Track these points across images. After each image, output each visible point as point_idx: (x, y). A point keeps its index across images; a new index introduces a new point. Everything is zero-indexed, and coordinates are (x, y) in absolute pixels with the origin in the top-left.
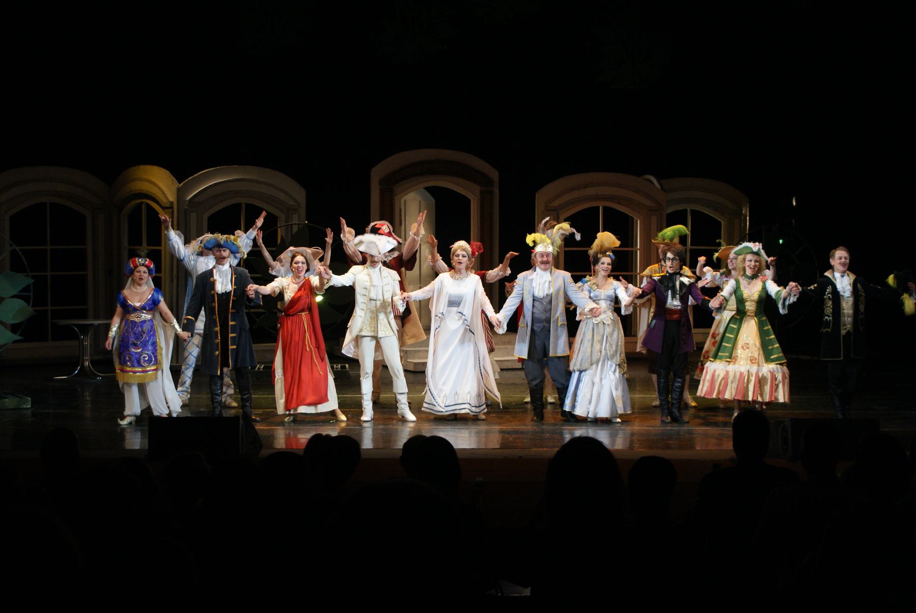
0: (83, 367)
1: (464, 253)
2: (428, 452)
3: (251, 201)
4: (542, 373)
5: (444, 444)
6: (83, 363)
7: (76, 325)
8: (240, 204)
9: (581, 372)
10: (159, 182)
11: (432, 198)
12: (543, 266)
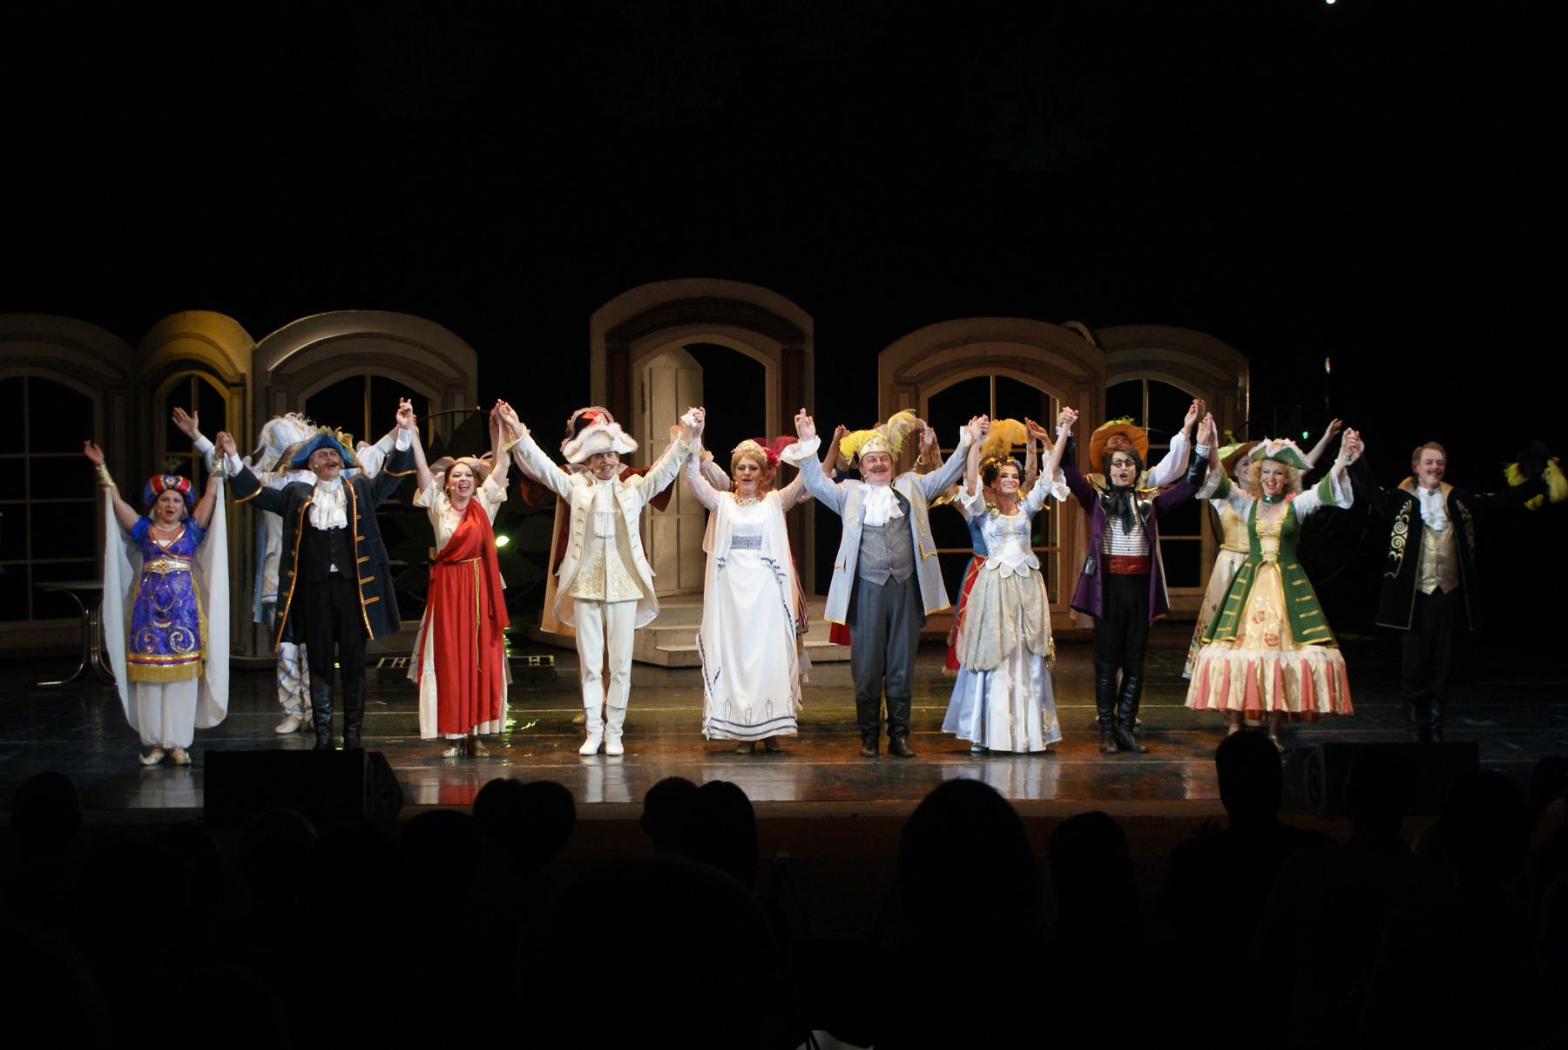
0: (88, 664)
1: (754, 464)
2: (690, 814)
4: (890, 655)
5: (731, 793)
6: (89, 658)
7: (76, 591)
8: (361, 379)
9: (985, 673)
10: (220, 341)
11: (698, 365)
12: (876, 477)
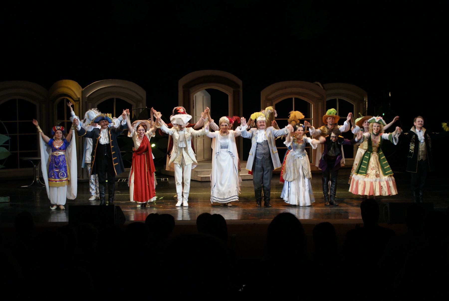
0: (35, 181)
3: (342, 98)
5: (219, 217)
6: (36, 179)
7: (31, 160)
8: (113, 99)
10: (73, 88)
